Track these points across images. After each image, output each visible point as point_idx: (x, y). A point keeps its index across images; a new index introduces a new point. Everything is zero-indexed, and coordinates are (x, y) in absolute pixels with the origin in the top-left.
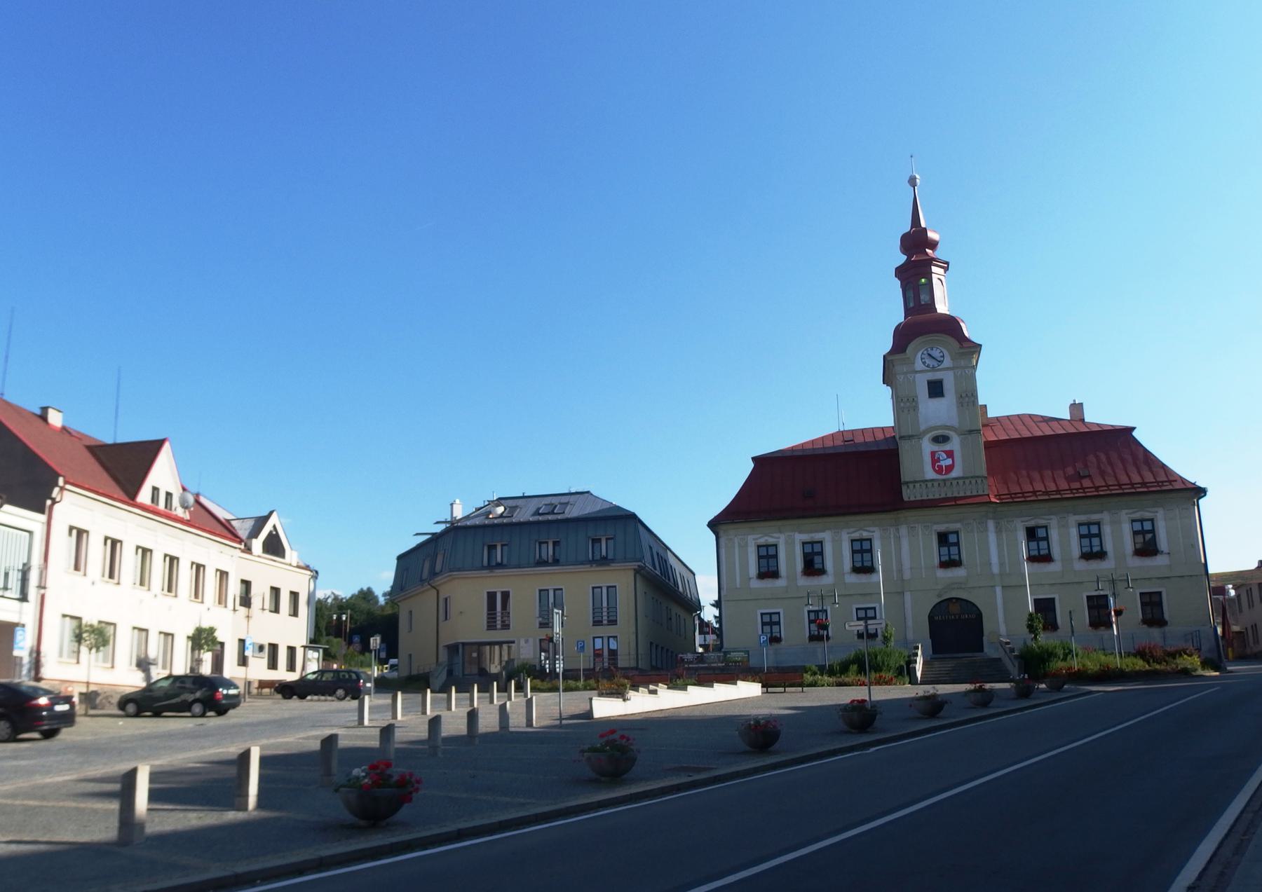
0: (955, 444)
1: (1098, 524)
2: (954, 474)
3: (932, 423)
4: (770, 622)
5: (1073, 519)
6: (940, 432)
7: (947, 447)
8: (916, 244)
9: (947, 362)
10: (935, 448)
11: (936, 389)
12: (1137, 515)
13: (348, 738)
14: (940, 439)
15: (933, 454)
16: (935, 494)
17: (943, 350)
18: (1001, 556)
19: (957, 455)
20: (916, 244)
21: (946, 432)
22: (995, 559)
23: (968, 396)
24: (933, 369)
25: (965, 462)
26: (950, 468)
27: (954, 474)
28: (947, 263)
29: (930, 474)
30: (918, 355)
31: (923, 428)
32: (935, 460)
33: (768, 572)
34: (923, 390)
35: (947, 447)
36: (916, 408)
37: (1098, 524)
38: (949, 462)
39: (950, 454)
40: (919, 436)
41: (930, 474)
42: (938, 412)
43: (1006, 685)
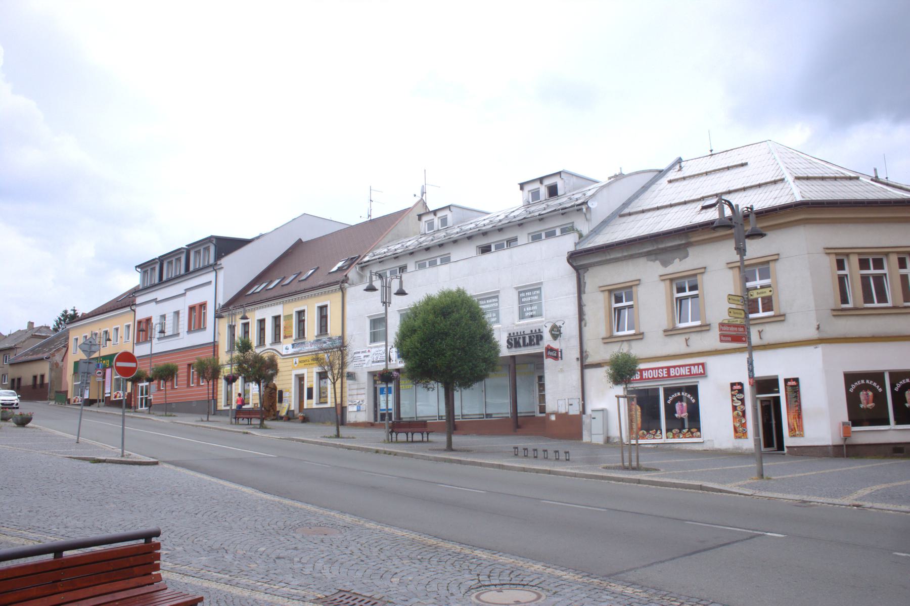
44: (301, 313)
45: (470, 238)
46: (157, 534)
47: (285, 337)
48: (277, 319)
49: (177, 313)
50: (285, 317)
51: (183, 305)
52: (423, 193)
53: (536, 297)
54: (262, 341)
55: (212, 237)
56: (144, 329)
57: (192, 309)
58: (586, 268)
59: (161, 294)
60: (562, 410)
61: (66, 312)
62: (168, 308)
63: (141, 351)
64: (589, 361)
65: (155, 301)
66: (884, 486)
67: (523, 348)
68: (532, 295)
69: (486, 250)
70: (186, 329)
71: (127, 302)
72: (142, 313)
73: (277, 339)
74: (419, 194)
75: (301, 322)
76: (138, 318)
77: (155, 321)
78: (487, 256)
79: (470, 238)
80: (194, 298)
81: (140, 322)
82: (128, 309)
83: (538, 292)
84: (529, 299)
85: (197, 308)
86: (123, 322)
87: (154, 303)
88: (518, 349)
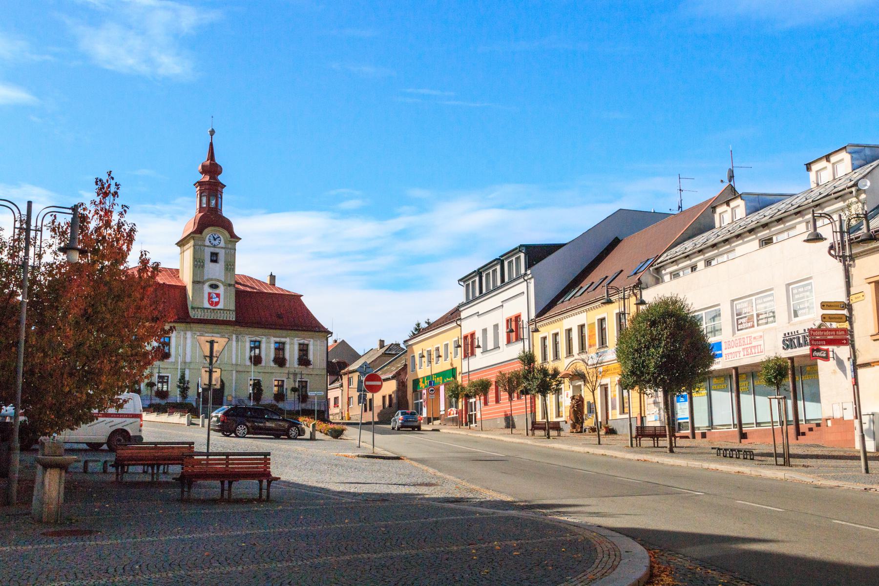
0: (221, 290)
1: (260, 342)
2: (218, 307)
3: (210, 277)
4: (257, 385)
5: (273, 339)
6: (213, 282)
7: (217, 291)
8: (212, 169)
9: (222, 244)
10: (211, 291)
11: (214, 258)
12: (254, 339)
13: (68, 431)
14: (214, 286)
15: (209, 294)
16: (208, 316)
17: (223, 235)
18: (237, 356)
19: (222, 297)
20: (212, 169)
21: (218, 283)
22: (234, 356)
23: (230, 266)
24: (214, 246)
25: (226, 302)
26: (217, 303)
27: (218, 307)
28: (508, 321)
29: (207, 305)
30: (208, 233)
31: (206, 278)
32: (210, 298)
33: (257, 360)
34: (207, 257)
35: (217, 291)
36: (203, 266)
37: (260, 342)
38: (217, 300)
39: (218, 295)
40: (203, 283)
41: (207, 305)
42: (214, 271)
43: (442, 408)
44: (602, 321)
45: (751, 231)
46: (269, 454)
47: (590, 346)
48: (582, 327)
49: (496, 327)
50: (589, 325)
51: (500, 318)
52: (731, 177)
53: (808, 293)
54: (556, 356)
55: (521, 246)
56: (469, 345)
57: (508, 321)
58: (852, 258)
59: (482, 306)
60: (838, 415)
61: (418, 325)
62: (488, 322)
63: (464, 366)
64: (859, 362)
65: (477, 314)
66: (587, 449)
67: (798, 349)
68: (804, 291)
69: (767, 241)
70: (505, 342)
71: (454, 316)
72: (467, 327)
73: (556, 356)
74: (726, 179)
75: (602, 330)
76: (464, 333)
77: (479, 335)
78: (769, 248)
79: (751, 231)
80: (511, 310)
81: (466, 337)
82: (454, 324)
83: (810, 287)
84: (801, 295)
85: (469, 337)
86: (449, 336)
87: (476, 317)
88: (794, 350)
